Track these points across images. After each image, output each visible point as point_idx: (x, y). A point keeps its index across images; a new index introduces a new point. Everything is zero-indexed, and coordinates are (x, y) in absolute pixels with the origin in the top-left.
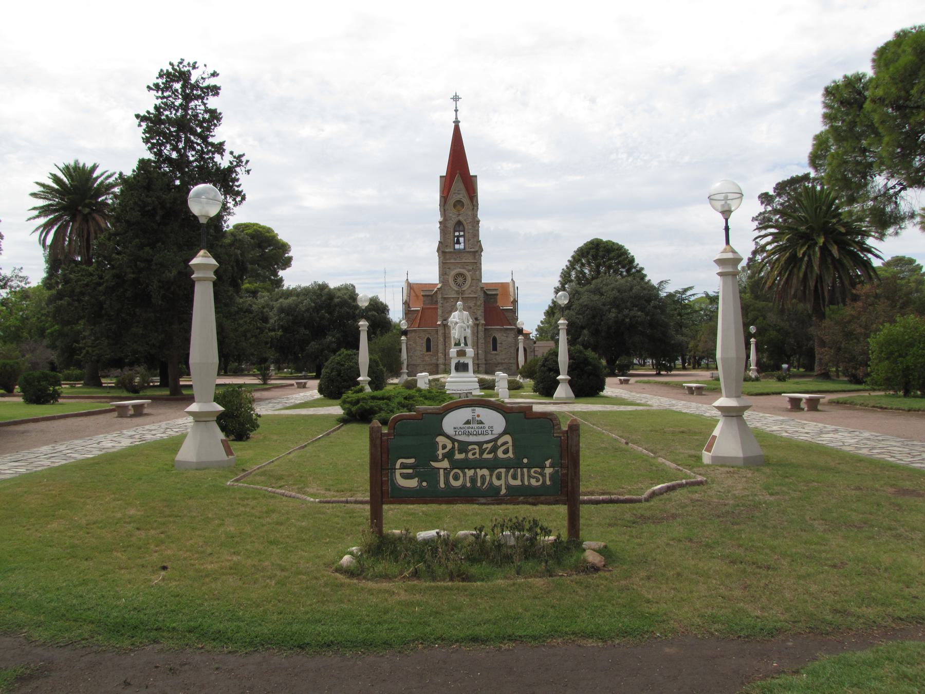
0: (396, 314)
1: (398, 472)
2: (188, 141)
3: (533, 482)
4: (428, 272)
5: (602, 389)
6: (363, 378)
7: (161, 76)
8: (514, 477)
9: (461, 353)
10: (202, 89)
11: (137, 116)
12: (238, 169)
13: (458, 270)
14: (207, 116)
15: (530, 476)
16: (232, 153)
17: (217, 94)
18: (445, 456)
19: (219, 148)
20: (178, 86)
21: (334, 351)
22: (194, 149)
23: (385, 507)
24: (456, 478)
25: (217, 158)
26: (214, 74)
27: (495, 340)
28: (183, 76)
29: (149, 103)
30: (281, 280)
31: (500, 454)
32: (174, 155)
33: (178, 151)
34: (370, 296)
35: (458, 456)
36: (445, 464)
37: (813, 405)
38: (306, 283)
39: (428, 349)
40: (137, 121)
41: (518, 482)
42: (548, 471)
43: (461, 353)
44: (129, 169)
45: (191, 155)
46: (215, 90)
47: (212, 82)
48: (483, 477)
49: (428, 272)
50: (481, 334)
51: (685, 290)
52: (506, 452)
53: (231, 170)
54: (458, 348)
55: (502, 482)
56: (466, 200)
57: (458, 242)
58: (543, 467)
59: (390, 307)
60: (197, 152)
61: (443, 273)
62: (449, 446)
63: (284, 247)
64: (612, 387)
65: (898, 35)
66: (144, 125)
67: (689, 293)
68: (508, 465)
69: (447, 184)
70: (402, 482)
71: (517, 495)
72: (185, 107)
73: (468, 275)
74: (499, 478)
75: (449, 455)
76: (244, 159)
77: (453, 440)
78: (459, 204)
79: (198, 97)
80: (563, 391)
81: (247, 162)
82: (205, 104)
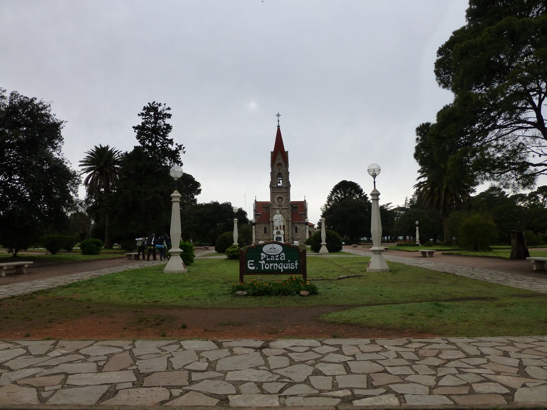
0: (250, 216)
1: (248, 265)
2: (156, 138)
3: (292, 268)
4: (266, 197)
5: (341, 249)
6: (236, 243)
7: (145, 109)
8: (286, 266)
9: (278, 233)
10: (163, 115)
11: (134, 127)
12: (180, 151)
13: (279, 195)
14: (165, 127)
15: (290, 266)
16: (177, 144)
17: (170, 118)
18: (263, 259)
19: (171, 142)
20: (152, 113)
21: (221, 233)
22: (159, 141)
23: (244, 276)
24: (267, 266)
25: (170, 146)
26: (169, 109)
27: (296, 228)
28: (155, 109)
29: (139, 121)
30: (196, 200)
31: (281, 259)
32: (150, 144)
33: (152, 142)
34: (239, 208)
35: (267, 259)
36: (264, 262)
37: (431, 254)
38: (208, 202)
39: (265, 232)
40: (134, 130)
41: (287, 268)
42: (296, 264)
43: (278, 233)
44: (130, 150)
45: (158, 145)
46: (169, 116)
47: (168, 112)
48: (276, 266)
49: (266, 197)
50: (290, 225)
51: (388, 204)
52: (283, 258)
53: (177, 151)
54: (277, 231)
55: (282, 268)
56: (283, 163)
57: (279, 183)
58: (295, 263)
59: (248, 213)
60: (161, 143)
61: (272, 197)
62: (265, 256)
63: (198, 184)
64: (346, 249)
65: (444, 108)
66: (137, 131)
67: (389, 206)
68: (283, 262)
69: (274, 156)
70: (250, 268)
71: (286, 272)
72: (155, 123)
73: (284, 198)
74: (281, 266)
75: (265, 259)
76: (182, 147)
77: (266, 254)
78: (280, 164)
79: (160, 118)
80: (324, 249)
81: (184, 148)
82: (164, 122)
